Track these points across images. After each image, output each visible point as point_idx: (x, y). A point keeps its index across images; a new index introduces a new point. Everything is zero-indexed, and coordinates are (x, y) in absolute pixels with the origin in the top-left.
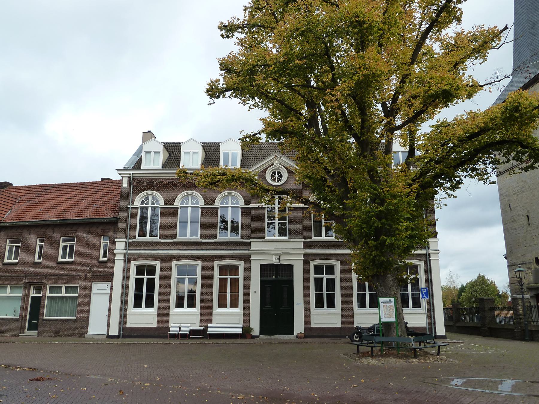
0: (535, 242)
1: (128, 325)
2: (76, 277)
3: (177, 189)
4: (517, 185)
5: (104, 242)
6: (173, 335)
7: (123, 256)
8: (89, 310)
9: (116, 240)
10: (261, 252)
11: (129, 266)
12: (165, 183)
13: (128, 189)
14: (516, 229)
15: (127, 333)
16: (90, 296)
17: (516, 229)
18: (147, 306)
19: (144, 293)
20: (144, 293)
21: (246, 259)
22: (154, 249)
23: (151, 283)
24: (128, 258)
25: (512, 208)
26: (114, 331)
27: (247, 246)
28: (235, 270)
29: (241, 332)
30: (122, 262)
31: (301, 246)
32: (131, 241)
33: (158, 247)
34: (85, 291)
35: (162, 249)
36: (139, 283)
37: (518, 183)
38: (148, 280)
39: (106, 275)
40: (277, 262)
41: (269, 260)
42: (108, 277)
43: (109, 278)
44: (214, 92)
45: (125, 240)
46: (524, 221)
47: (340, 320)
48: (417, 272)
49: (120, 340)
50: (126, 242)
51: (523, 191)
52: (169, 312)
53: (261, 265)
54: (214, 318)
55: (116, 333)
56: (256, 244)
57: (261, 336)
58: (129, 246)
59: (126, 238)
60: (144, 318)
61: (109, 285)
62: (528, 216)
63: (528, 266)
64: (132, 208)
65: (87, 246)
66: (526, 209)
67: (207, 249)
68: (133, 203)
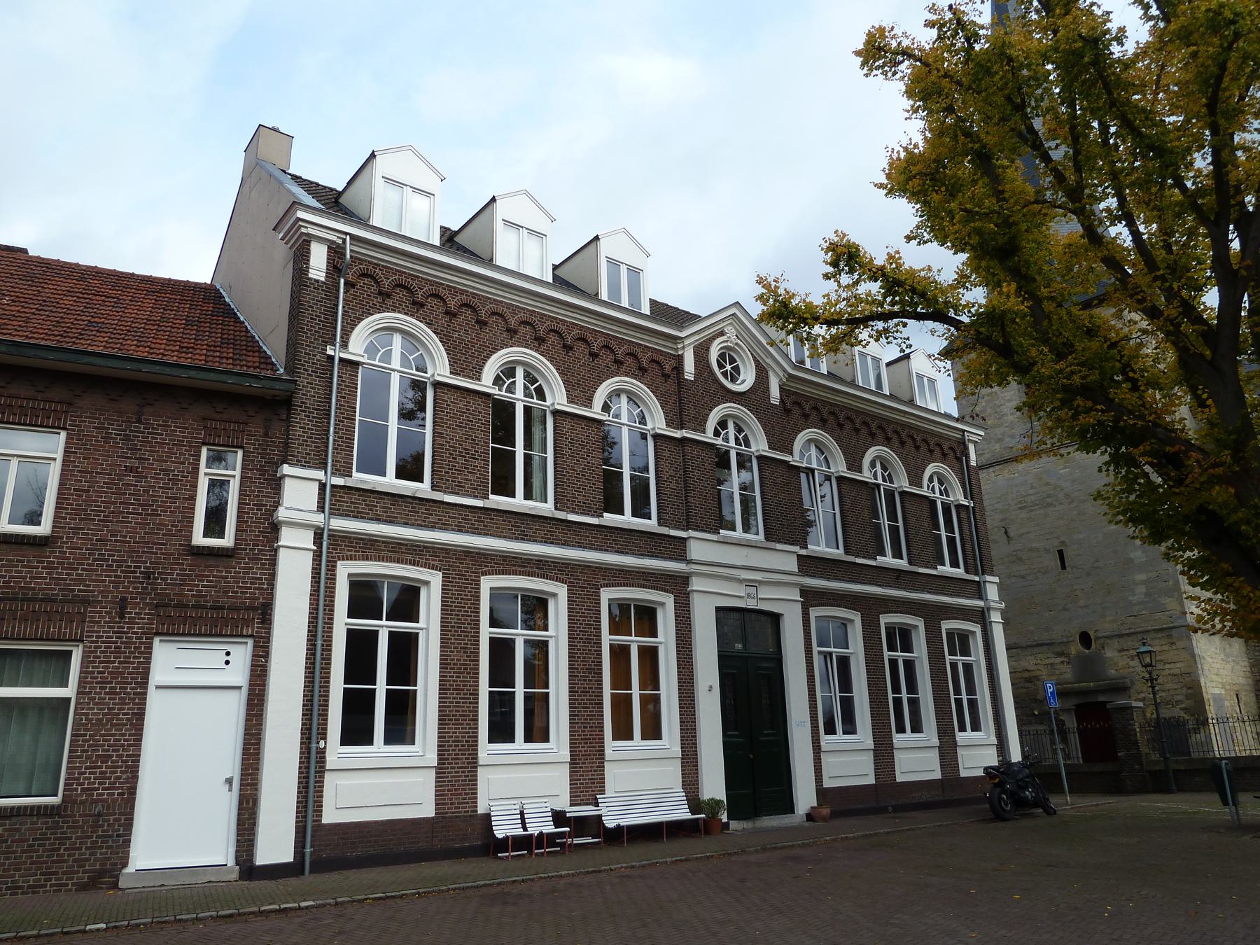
0: (1082, 603)
1: (330, 816)
2: (69, 608)
3: (486, 334)
4: (1032, 491)
5: (218, 475)
6: (504, 844)
7: (311, 534)
8: (136, 759)
9: (286, 469)
10: (717, 570)
11: (332, 579)
12: (452, 303)
13: (330, 288)
14: (1023, 577)
15: (331, 850)
16: (143, 696)
17: (1023, 577)
18: (528, 738)
19: (381, 687)
20: (381, 687)
21: (678, 585)
22: (420, 526)
23: (404, 648)
24: (330, 547)
25: (1011, 534)
26: (276, 845)
27: (677, 549)
28: (647, 618)
29: (428, 811)
30: (308, 559)
31: (792, 565)
32: (339, 481)
33: (435, 519)
34: (116, 673)
35: (445, 527)
36: (361, 645)
37: (1032, 488)
38: (393, 636)
39: (232, 608)
40: (751, 604)
41: (737, 596)
42: (247, 617)
43: (247, 622)
44: (877, 52)
45: (320, 475)
46: (1053, 562)
47: (872, 766)
48: (907, 647)
49: (308, 878)
50: (322, 487)
51: (1050, 505)
52: (475, 757)
53: (718, 609)
54: (610, 771)
55: (285, 854)
56: (701, 547)
57: (734, 825)
58: (338, 500)
59: (323, 466)
60: (384, 784)
61: (242, 653)
62: (1061, 553)
63: (1058, 649)
64: (341, 360)
65: (130, 479)
66: (1058, 538)
67: (580, 546)
68: (345, 345)
